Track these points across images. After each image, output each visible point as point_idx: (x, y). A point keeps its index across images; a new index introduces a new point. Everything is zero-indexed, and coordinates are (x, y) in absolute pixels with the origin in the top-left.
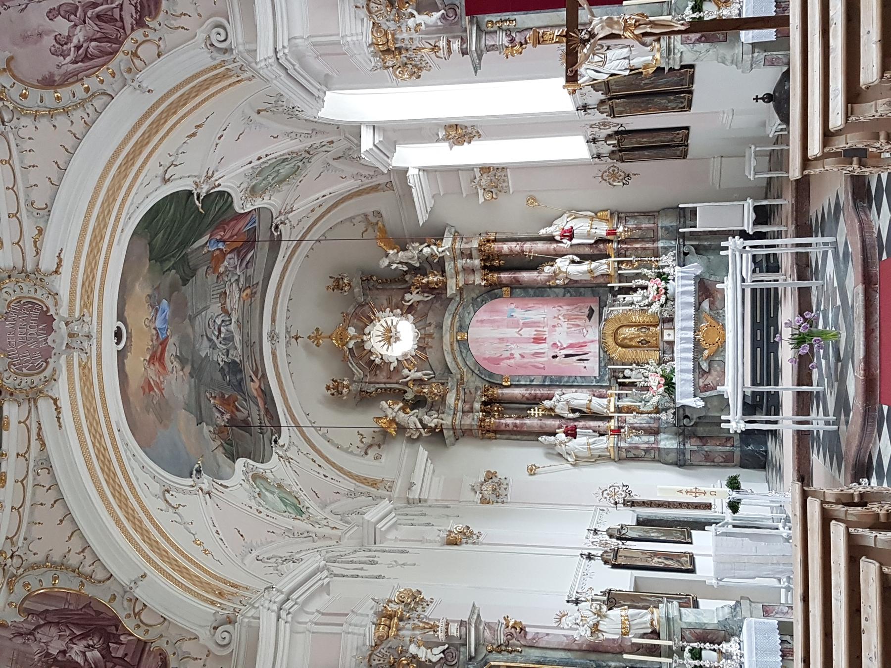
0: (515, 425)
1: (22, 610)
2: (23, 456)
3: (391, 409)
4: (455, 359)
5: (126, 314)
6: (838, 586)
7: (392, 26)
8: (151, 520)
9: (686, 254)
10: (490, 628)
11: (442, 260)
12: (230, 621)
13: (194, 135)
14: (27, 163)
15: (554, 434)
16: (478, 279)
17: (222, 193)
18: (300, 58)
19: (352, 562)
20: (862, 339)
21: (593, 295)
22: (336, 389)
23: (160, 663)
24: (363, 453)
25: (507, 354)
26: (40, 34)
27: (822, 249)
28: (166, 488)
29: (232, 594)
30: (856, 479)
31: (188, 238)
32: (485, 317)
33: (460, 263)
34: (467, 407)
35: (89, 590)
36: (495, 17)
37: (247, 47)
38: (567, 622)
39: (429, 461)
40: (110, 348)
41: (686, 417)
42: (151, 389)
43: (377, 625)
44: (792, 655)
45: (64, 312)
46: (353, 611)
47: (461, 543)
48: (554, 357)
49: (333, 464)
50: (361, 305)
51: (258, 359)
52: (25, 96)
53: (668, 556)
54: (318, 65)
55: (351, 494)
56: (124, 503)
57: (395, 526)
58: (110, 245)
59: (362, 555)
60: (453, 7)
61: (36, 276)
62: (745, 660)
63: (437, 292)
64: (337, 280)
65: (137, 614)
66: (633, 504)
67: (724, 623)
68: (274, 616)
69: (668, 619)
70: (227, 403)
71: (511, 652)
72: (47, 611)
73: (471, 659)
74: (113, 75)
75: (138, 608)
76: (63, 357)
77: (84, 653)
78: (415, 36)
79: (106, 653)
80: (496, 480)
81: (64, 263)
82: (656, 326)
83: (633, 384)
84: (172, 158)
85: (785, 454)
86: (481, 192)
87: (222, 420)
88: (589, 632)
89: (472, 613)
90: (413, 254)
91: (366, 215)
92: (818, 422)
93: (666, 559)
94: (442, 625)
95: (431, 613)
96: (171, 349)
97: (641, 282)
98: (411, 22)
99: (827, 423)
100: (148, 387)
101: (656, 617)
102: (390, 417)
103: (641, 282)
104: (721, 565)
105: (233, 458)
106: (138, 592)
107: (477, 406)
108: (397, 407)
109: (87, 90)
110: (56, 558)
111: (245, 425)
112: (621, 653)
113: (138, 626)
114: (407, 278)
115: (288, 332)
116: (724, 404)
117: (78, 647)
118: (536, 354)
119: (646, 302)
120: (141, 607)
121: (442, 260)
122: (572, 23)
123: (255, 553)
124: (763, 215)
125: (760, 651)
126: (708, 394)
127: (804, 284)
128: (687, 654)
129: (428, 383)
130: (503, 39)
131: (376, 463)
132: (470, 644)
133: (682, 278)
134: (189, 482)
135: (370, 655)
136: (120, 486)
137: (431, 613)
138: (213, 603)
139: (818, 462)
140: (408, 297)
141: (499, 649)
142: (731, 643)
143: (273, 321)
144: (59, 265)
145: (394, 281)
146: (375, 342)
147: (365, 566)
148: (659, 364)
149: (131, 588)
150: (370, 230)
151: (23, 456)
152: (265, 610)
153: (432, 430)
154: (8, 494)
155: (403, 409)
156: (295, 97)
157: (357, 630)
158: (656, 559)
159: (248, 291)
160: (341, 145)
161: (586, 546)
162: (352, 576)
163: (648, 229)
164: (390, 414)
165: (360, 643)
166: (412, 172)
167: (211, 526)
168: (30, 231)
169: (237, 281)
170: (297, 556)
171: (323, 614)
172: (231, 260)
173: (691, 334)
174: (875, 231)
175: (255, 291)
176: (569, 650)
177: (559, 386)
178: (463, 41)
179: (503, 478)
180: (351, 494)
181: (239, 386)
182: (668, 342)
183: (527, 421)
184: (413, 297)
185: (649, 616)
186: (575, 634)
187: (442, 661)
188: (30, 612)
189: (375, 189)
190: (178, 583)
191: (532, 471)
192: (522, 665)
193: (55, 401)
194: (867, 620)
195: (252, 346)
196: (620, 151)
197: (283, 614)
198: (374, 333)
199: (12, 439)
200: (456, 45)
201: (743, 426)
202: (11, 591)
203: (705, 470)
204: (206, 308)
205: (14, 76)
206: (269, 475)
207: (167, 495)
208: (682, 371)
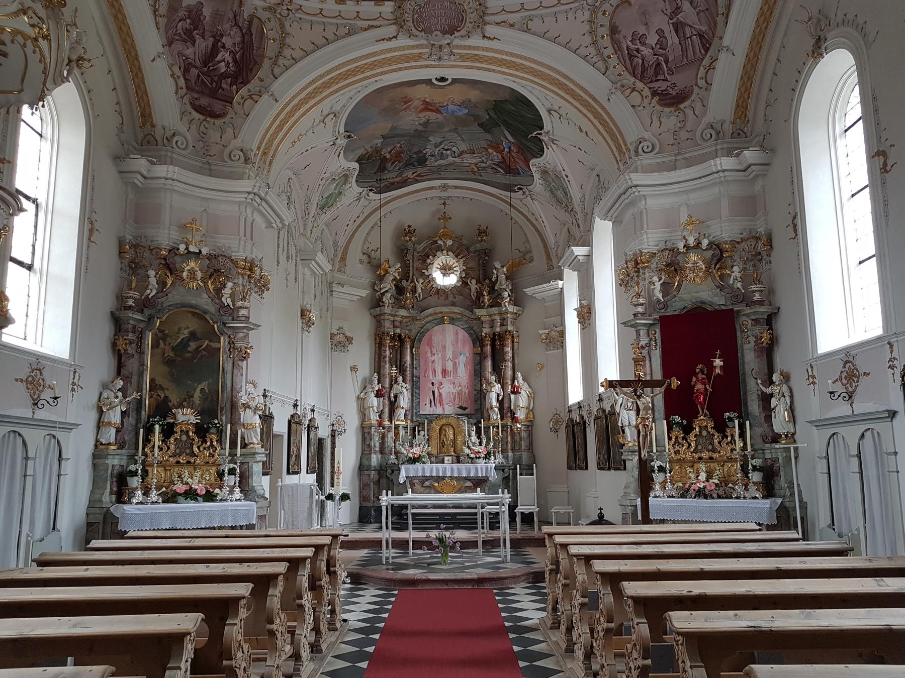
0: (385, 357)
1: (252, 17)
2: (358, 16)
3: (395, 271)
4: (431, 315)
5: (457, 84)
6: (273, 552)
7: (654, 266)
8: (315, 105)
9: (503, 470)
11: (499, 305)
12: (247, 160)
13: (581, 131)
14: (559, 16)
15: (379, 382)
16: (486, 330)
18: (632, 203)
20: (441, 578)
21: (475, 409)
22: (409, 231)
25: (434, 351)
26: (646, 24)
27: (503, 554)
29: (265, 162)
30: (350, 575)
31: (511, 126)
32: (460, 336)
33: (497, 318)
34: (397, 324)
35: (266, 64)
36: (658, 336)
38: (250, 388)
40: (432, 74)
41: (393, 472)
42: (406, 103)
43: (245, 261)
45: (457, 42)
48: (433, 384)
49: (356, 231)
50: (468, 249)
51: (429, 177)
52: (604, 14)
53: (298, 457)
54: (628, 215)
55: (335, 244)
56: (326, 85)
57: (314, 274)
58: (504, 73)
59: (293, 251)
60: (665, 306)
61: (481, 22)
62: (229, 503)
63: (478, 303)
64: (485, 232)
65: (250, 97)
66: (333, 436)
68: (250, 190)
69: (254, 454)
70: (398, 156)
73: (224, 324)
74: (620, 75)
75: (255, 97)
76: (426, 42)
77: (223, 60)
78: (647, 282)
79: (224, 76)
81: (490, 42)
82: (454, 451)
83: (414, 437)
85: (368, 534)
86: (546, 331)
87: (385, 152)
89: (254, 325)
90: (503, 284)
91: (530, 251)
92: (388, 553)
94: (246, 304)
95: (254, 297)
96: (433, 116)
97: (484, 442)
98: (656, 279)
99: (387, 558)
100: (407, 101)
101: (256, 446)
102: (390, 270)
103: (484, 442)
105: (359, 160)
106: (265, 97)
107: (398, 331)
108: (396, 275)
109: (609, 57)
110: (287, 41)
111: (382, 169)
112: (231, 423)
113: (243, 98)
114: (487, 281)
115: (448, 198)
116: (401, 490)
117: (228, 57)
118: (434, 371)
119: (471, 445)
121: (499, 305)
122: (652, 384)
123: (293, 177)
124: (528, 519)
126: (409, 485)
127: (480, 544)
128: (232, 466)
129: (414, 297)
130: (644, 341)
131: (357, 261)
133: (487, 468)
134: (342, 130)
136: (337, 83)
137: (254, 297)
138: (259, 148)
139: (363, 553)
140: (474, 281)
141: (231, 343)
143: (456, 187)
144: (489, 38)
145: (485, 271)
146: (442, 259)
147: (285, 252)
148: (428, 454)
150: (521, 254)
151: (358, 16)
153: (380, 300)
154: (331, 6)
155: (395, 279)
156: (607, 199)
157: (242, 246)
159: (476, 169)
160: (577, 233)
163: (521, 445)
164: (391, 270)
166: (560, 283)
168: (512, 18)
169: (483, 162)
170: (292, 207)
172: (497, 157)
173: (448, 474)
174: (513, 586)
175: (476, 174)
177: (412, 387)
178: (643, 314)
180: (335, 244)
181: (409, 164)
182: (443, 459)
183: (388, 365)
184: (473, 285)
185: (256, 442)
186: (243, 393)
188: (250, 23)
189: (549, 258)
190: (272, 124)
191: (354, 369)
193: (395, 37)
195: (438, 173)
196: (573, 426)
197: (251, 196)
198: (449, 258)
199: (369, 8)
200: (640, 309)
201: (384, 504)
202: (264, 9)
203: (357, 483)
204: (463, 140)
205: (618, 6)
206: (348, 186)
207: (332, 116)
208: (424, 469)
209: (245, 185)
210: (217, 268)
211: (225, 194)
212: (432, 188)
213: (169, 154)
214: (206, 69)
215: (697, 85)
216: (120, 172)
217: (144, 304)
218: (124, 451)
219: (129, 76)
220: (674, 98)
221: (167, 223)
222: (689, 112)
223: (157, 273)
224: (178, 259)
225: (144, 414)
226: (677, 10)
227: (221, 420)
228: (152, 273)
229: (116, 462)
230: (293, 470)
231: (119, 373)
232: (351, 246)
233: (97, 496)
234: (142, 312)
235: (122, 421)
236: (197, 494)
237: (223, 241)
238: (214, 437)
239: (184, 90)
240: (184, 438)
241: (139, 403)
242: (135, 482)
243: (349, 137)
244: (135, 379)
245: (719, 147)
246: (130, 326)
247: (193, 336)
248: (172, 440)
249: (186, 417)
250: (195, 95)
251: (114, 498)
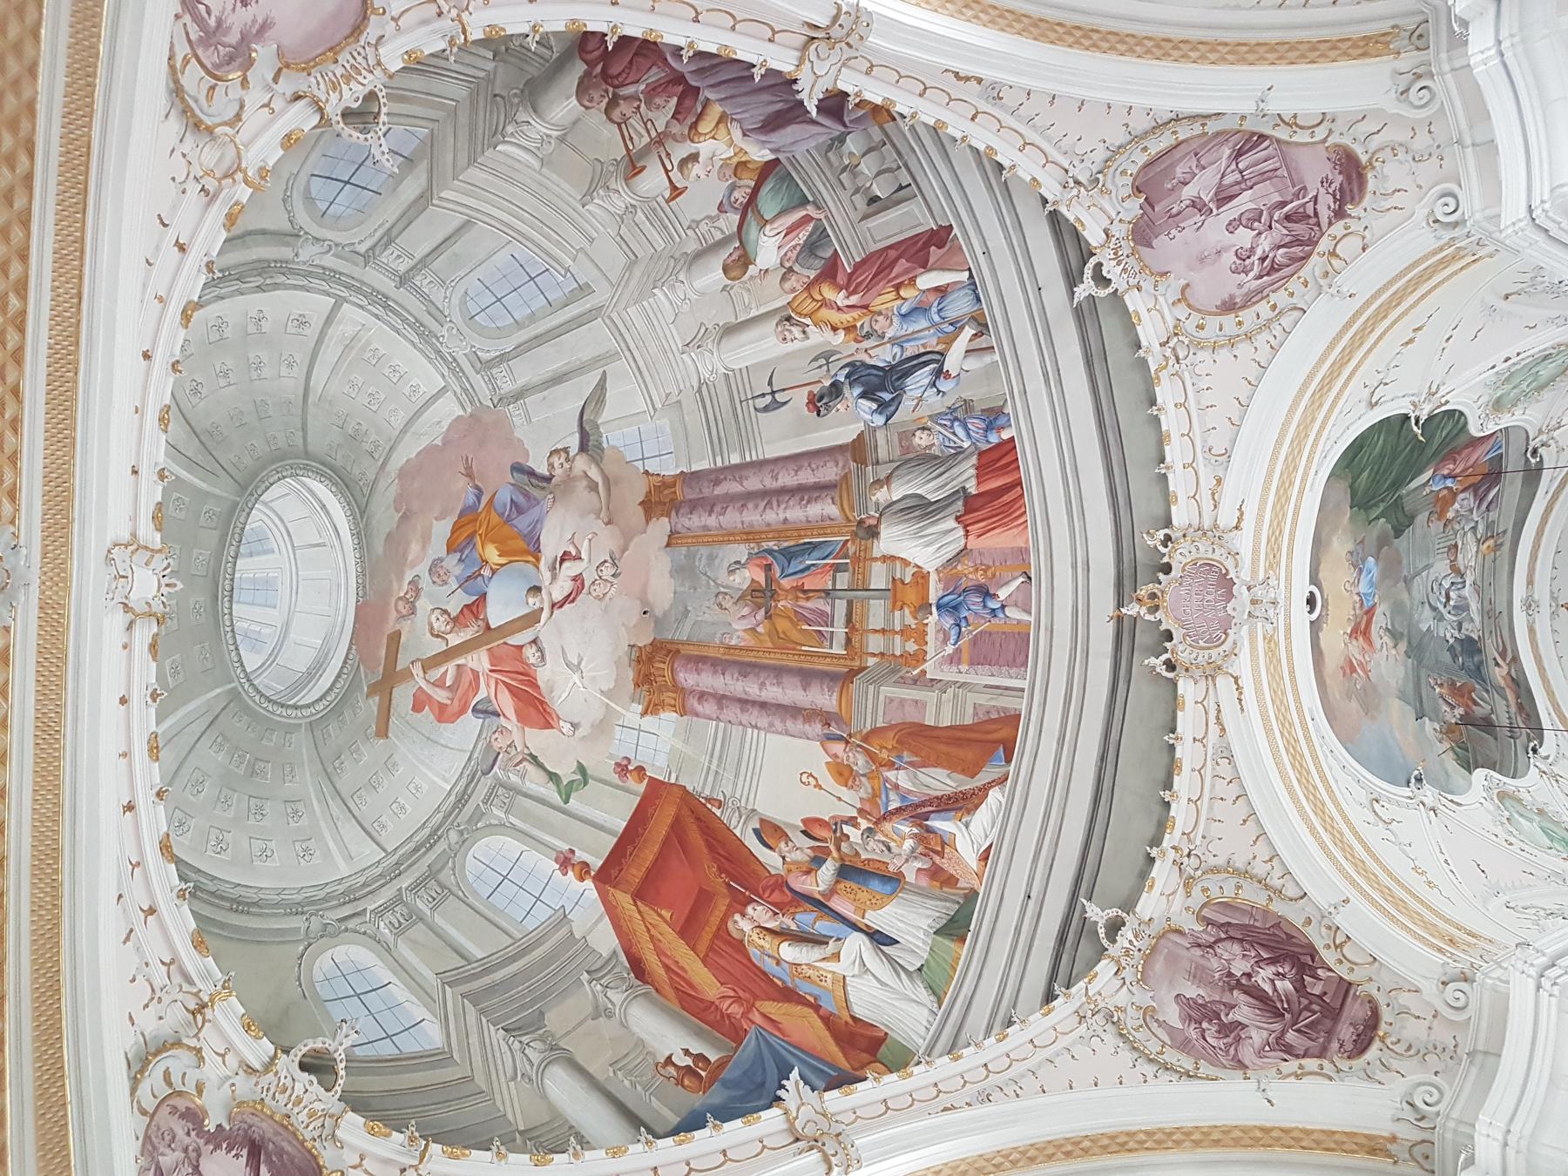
1: (1202, 919)
13: (1411, 341)
17: (1451, 413)
29: (1469, 945)
37: (1488, 212)
68: (1531, 984)
72: (1229, 924)
74: (1306, 284)
77: (1272, 981)
79: (1300, 987)
84: (1381, 376)
106: (1338, 920)
109: (1274, 307)
134: (1406, 792)
138: (1440, 950)
143: (1530, 582)
197: (1546, 983)
204: (1428, 567)
205: (1189, 306)
206: (1524, 795)
209: (1521, 992)
212: (1531, 630)
213: (1451, 1124)
214: (1287, 1016)
215: (1325, 140)
220: (1349, 179)
222: (1375, 142)
226: (1197, 205)
239: (1325, 1063)
243: (1419, 780)
245: (1446, 67)
250: (1335, 1045)
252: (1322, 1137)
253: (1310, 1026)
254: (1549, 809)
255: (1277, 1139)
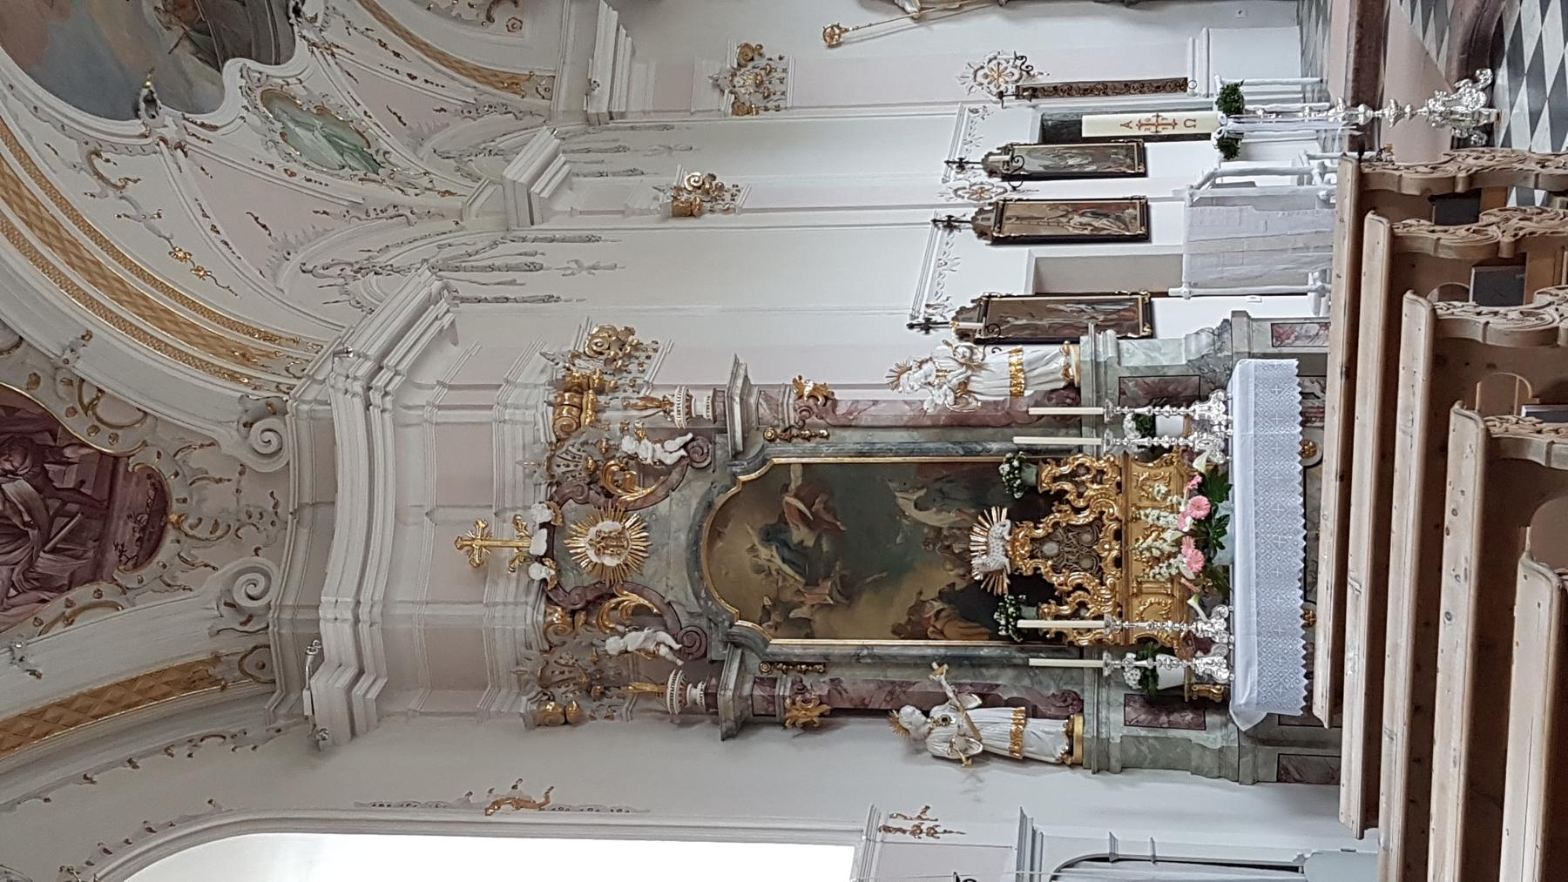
6: (1409, 409)
10: (768, 399)
19: (492, 268)
23: (152, 493)
24: (483, 17)
28: (91, 147)
29: (267, 355)
39: (623, 31)
44: (1322, 419)
46: (507, 381)
47: (701, 213)
53: (1099, 208)
62: (1235, 432)
65: (89, 408)
66: (1035, 93)
67: (1198, 364)
68: (358, 403)
69: (1096, 365)
71: (808, 439)
73: (736, 455)
75: (90, 401)
79: (42, 483)
80: (763, 63)
88: (951, 399)
89: (734, 376)
93: (1096, 215)
94: (678, 400)
101: (1074, 359)
104: (1199, 260)
106: (81, 368)
113: (96, 429)
120: (94, 393)
123: (296, 259)
125: (1263, 417)
128: (1128, 423)
131: (512, 39)
132: (734, 431)
134: (136, 127)
135: (549, 459)
138: (233, 377)
142: (1210, 403)
149: (67, 361)
152: (340, 395)
158: (1077, 219)
161: (943, 201)
162: (496, 300)
165: (529, 438)
167: (200, 218)
171: (451, 387)
176: (915, 427)
179: (775, 57)
180: (471, 111)
185: (1062, 361)
187: (684, 462)
191: (834, 38)
192: (831, 460)
194: (1455, 512)
197: (375, 397)
206: (296, 89)
207: (97, 162)
209: (348, 418)
210: (588, 480)
211: (379, 453)
213: (287, 615)
214: (33, 533)
216: (353, 733)
217: (698, 659)
218: (1088, 697)
219: (90, 729)
221: (476, 610)
223: (614, 631)
224: (570, 581)
225: (988, 649)
227: (1001, 453)
228: (613, 645)
229: (1117, 717)
230: (1133, 223)
231: (884, 713)
232: (470, 60)
233: (1209, 760)
234: (718, 666)
235: (1008, 703)
236: (1210, 517)
237: (509, 467)
238: (1048, 471)
239: (104, 586)
240: (1050, 548)
241: (955, 662)
242: (1170, 671)
243: (150, 101)
244: (894, 675)
246: (758, 692)
247: (774, 535)
248: (1056, 580)
249: (994, 545)
250: (112, 555)
251: (1212, 719)
252: (118, 693)
253: (72, 536)
254: (330, 104)
255: (58, 719)
